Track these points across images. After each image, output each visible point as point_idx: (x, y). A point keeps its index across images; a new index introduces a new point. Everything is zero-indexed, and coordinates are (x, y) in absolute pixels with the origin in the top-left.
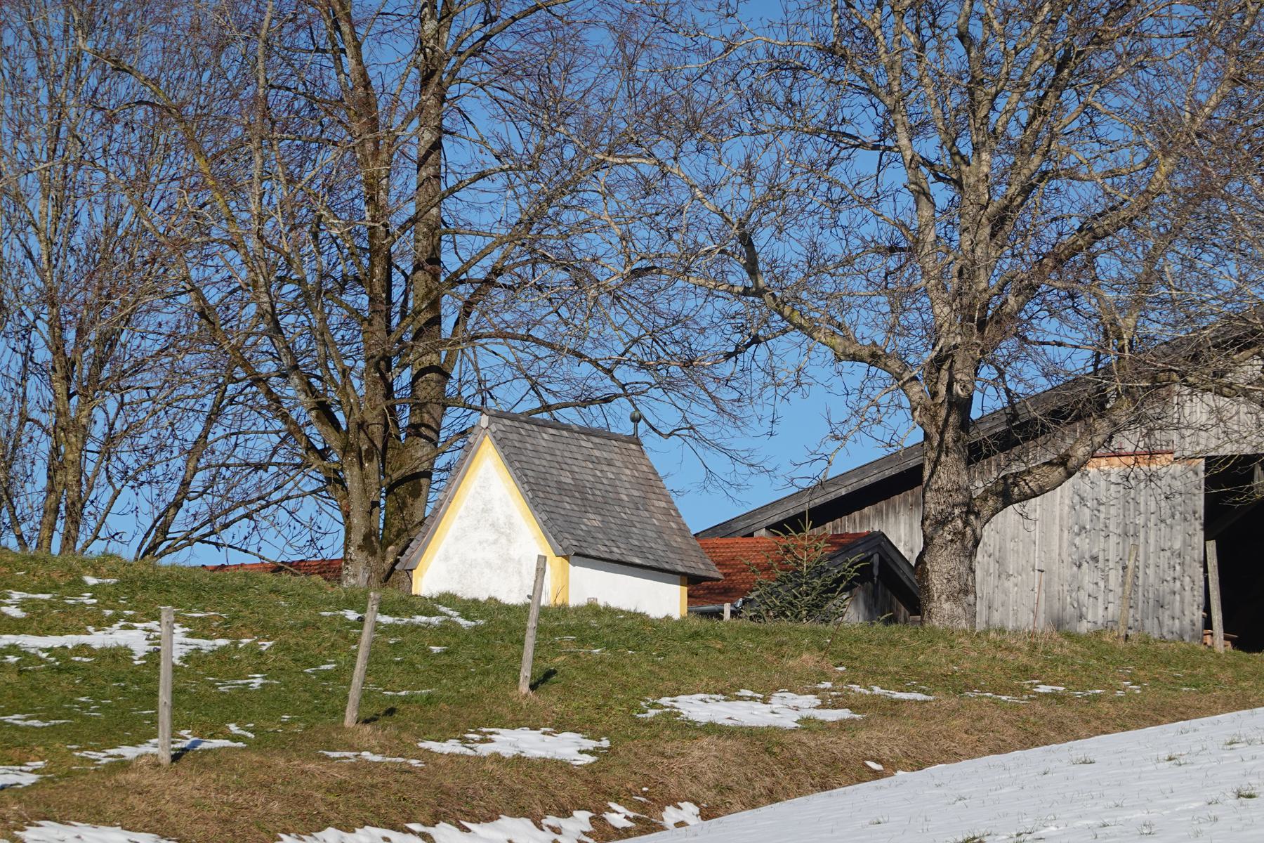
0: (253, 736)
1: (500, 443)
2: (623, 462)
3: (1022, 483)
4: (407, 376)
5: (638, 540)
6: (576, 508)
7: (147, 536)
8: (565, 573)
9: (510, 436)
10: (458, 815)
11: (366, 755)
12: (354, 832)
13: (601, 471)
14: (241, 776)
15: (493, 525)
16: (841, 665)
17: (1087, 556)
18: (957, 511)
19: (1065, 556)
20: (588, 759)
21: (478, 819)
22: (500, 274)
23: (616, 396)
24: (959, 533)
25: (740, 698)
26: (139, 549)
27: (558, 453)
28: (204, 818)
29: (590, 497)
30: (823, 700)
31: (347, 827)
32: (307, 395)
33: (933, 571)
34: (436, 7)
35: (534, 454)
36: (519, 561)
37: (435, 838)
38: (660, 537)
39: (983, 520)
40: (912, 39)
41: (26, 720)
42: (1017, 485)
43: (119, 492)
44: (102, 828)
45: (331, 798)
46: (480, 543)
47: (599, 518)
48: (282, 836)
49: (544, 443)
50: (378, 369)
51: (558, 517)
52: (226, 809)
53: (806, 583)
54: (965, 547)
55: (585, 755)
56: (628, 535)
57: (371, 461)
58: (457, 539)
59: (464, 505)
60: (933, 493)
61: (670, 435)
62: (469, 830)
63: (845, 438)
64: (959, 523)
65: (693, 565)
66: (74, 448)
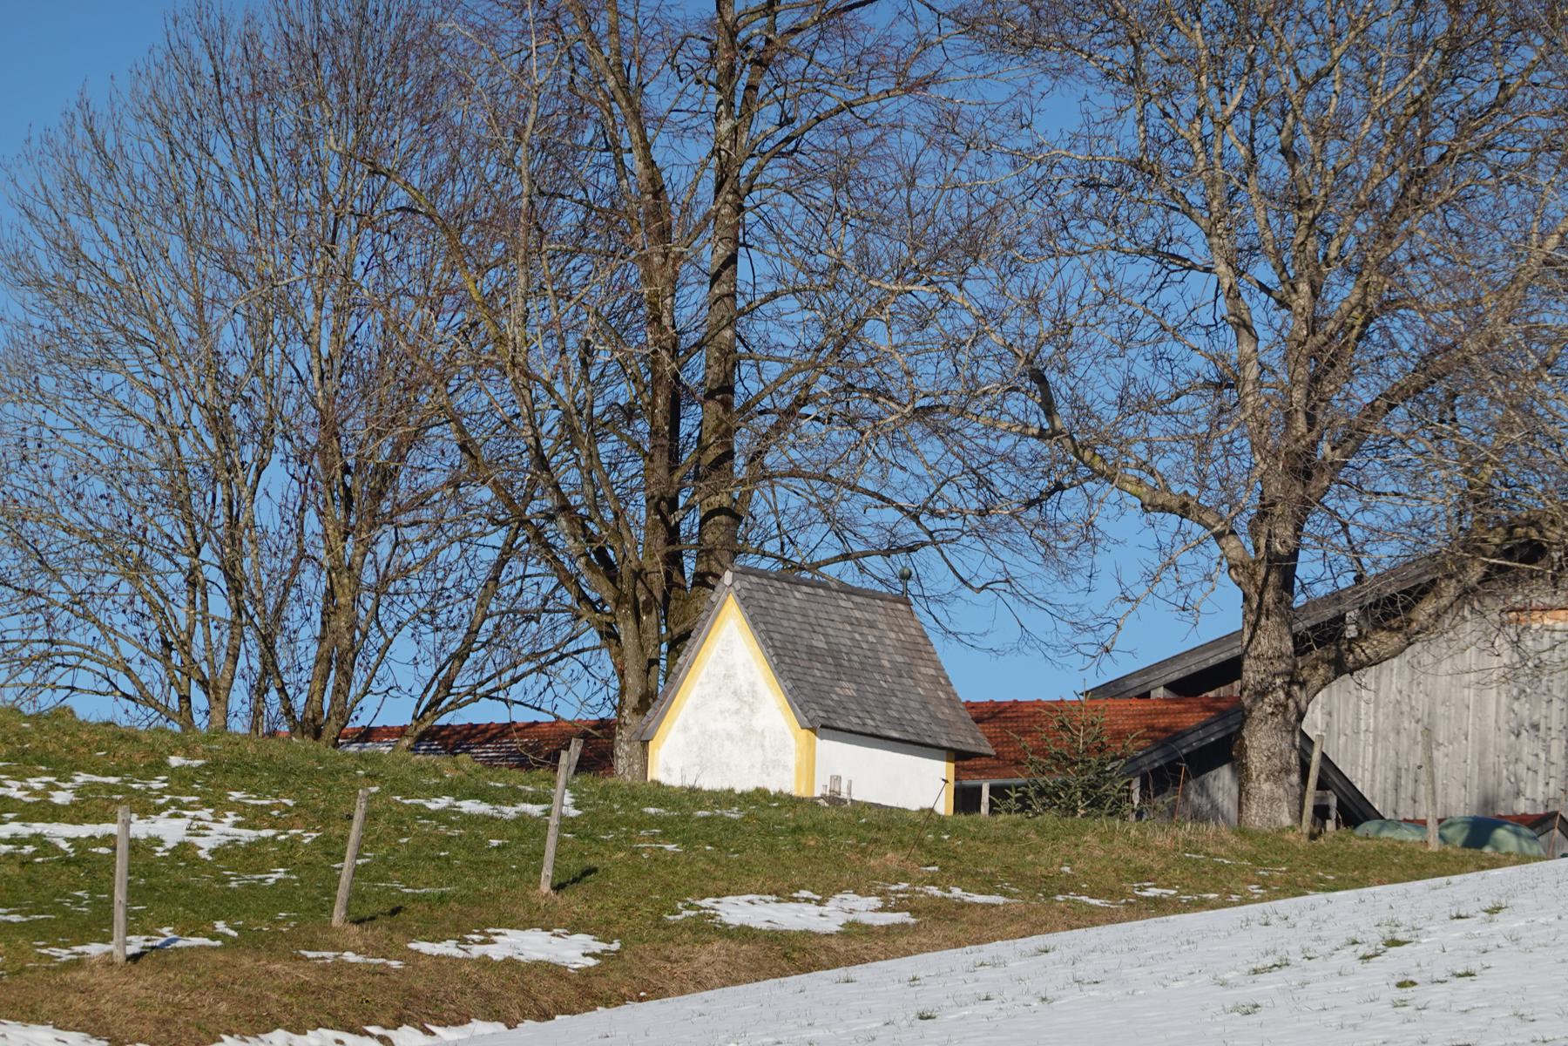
0: (236, 934)
1: (745, 602)
2: (888, 624)
3: (1358, 650)
4: (695, 517)
5: (898, 711)
6: (827, 675)
7: (427, 690)
8: (812, 746)
9: (756, 595)
10: (425, 1018)
11: (350, 957)
12: (305, 1034)
13: (861, 634)
14: (199, 976)
15: (735, 693)
16: (934, 864)
17: (1526, 724)
18: (1278, 681)
19: (1502, 723)
20: (591, 962)
21: (444, 1023)
22: (805, 404)
23: (923, 544)
24: (1281, 705)
25: (796, 900)
26: (418, 707)
27: (811, 613)
28: (144, 1017)
29: (846, 663)
30: (887, 901)
31: (299, 1029)
32: (576, 540)
33: (1252, 747)
34: (733, 105)
35: (783, 615)
36: (763, 732)
37: (394, 1041)
38: (924, 708)
39: (1311, 692)
40: (1242, 152)
41: (6, 914)
42: (1352, 652)
43: (391, 642)
44: (32, 1026)
45: (286, 999)
46: (722, 712)
47: (854, 686)
48: (224, 1037)
49: (796, 603)
50: (659, 511)
51: (805, 685)
52: (169, 1009)
53: (1083, 761)
54: (1287, 722)
55: (588, 958)
56: (886, 706)
57: (649, 613)
58: (697, 708)
59: (705, 669)
60: (1252, 661)
61: (982, 588)
62: (433, 1034)
63: (1137, 600)
64: (1281, 695)
65: (961, 739)
66: (347, 591)
